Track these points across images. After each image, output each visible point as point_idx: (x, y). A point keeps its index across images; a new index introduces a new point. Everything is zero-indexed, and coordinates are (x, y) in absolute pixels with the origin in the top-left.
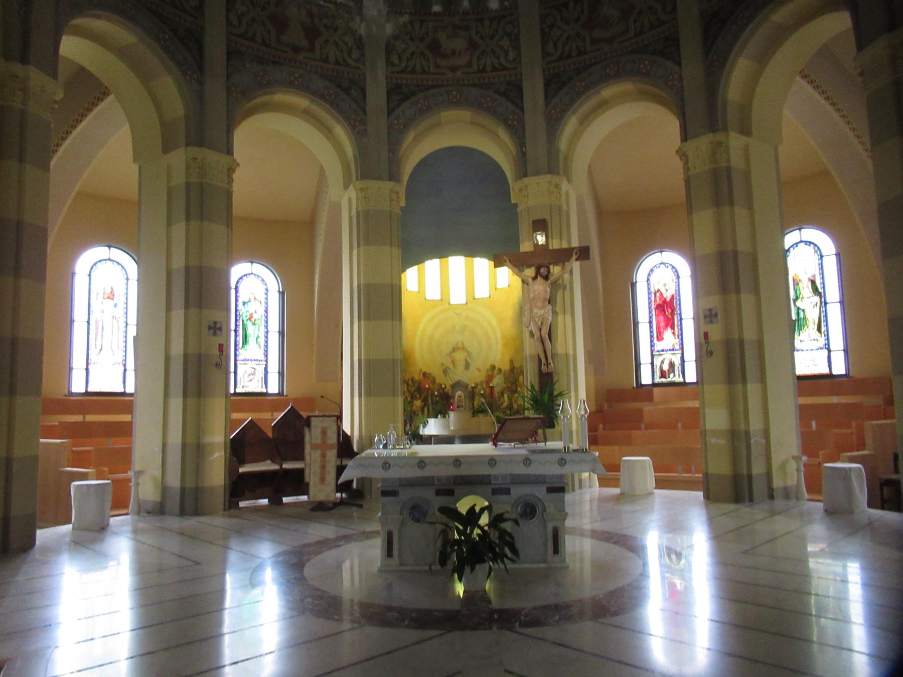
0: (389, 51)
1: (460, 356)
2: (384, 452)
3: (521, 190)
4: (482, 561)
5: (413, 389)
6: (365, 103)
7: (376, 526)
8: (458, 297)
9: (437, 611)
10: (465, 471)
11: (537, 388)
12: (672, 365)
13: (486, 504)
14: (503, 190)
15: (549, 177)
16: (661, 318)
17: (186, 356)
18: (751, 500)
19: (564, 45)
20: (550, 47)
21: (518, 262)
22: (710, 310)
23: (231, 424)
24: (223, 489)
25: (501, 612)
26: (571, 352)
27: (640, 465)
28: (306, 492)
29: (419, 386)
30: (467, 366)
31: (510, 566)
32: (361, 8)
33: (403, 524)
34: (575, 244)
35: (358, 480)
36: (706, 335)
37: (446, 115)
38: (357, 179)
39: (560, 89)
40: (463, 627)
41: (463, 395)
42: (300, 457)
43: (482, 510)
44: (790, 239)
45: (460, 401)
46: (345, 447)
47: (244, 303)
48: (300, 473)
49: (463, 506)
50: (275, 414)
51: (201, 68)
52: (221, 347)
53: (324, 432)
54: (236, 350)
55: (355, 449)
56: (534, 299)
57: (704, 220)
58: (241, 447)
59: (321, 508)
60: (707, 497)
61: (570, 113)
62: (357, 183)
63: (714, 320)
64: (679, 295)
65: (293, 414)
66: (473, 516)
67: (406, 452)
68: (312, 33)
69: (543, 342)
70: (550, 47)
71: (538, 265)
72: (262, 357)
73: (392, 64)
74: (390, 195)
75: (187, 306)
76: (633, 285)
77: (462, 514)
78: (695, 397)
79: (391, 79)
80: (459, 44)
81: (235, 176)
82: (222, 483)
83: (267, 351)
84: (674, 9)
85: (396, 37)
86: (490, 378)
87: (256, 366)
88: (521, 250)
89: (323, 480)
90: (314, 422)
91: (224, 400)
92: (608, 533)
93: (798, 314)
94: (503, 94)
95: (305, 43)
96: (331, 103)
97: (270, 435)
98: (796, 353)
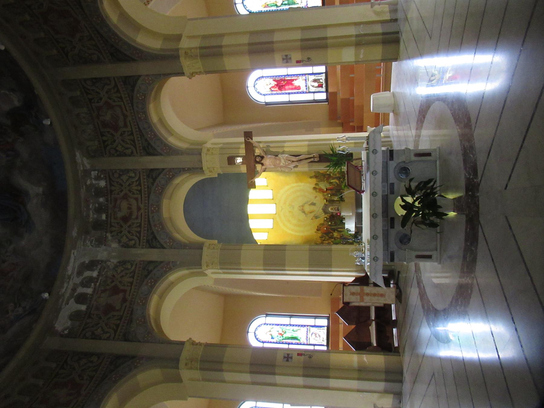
0: (126, 246)
1: (307, 208)
2: (367, 259)
3: (210, 171)
4: (435, 200)
5: (327, 238)
6: (157, 262)
7: (413, 264)
8: (272, 209)
9: (466, 229)
10: (379, 211)
11: (328, 164)
12: (315, 81)
13: (399, 197)
14: (211, 180)
15: (204, 157)
16: (287, 87)
17: (304, 376)
18: (398, 33)
19: (127, 143)
20: (128, 151)
21: (253, 173)
22: (283, 59)
23: (346, 350)
24: (386, 356)
25: (467, 189)
26: (307, 143)
27: (377, 100)
28: (390, 306)
29: (325, 234)
30: (313, 204)
31: (438, 184)
32: (102, 261)
33: (412, 249)
34: (242, 139)
35: (383, 273)
36: (298, 62)
37: (165, 214)
38: (201, 268)
39: (152, 146)
40: (477, 213)
41: (331, 207)
42: (368, 309)
43: (404, 201)
44: (242, 11)
45: (335, 209)
46: (362, 281)
47: (272, 338)
48: (377, 309)
49: (401, 212)
50: (340, 322)
51: (133, 357)
52: (298, 354)
53: (353, 294)
54: (301, 344)
55: (364, 275)
56: (275, 165)
57: (229, 63)
58: (360, 344)
59: (400, 297)
60: (396, 60)
61: (166, 142)
62: (203, 268)
63: (289, 57)
64: (273, 76)
65: (340, 312)
66: (407, 206)
67: (368, 247)
68: (116, 290)
69: (301, 160)
70: (128, 151)
71: (255, 162)
72: (305, 328)
73: (135, 244)
74: (211, 249)
75: (274, 374)
76: (267, 104)
77: (406, 213)
78: (335, 67)
79: (143, 245)
80: (124, 205)
81: (197, 341)
82: (383, 356)
83: (302, 326)
84: (108, 78)
85: (120, 242)
86: (321, 190)
87: (310, 333)
88: (246, 172)
89: (382, 295)
90: (346, 300)
91: (331, 354)
92: (418, 121)
93: (285, 4)
94: (154, 180)
95: (121, 295)
96: (156, 282)
97: (353, 327)
98: (309, 6)
